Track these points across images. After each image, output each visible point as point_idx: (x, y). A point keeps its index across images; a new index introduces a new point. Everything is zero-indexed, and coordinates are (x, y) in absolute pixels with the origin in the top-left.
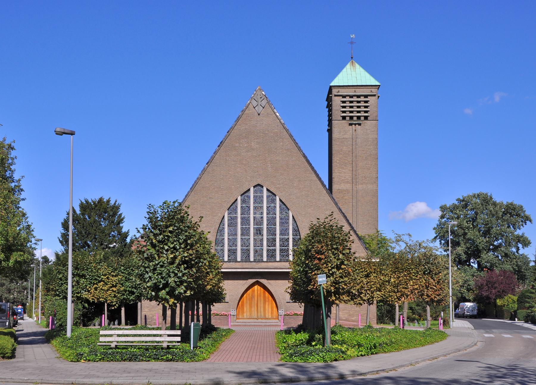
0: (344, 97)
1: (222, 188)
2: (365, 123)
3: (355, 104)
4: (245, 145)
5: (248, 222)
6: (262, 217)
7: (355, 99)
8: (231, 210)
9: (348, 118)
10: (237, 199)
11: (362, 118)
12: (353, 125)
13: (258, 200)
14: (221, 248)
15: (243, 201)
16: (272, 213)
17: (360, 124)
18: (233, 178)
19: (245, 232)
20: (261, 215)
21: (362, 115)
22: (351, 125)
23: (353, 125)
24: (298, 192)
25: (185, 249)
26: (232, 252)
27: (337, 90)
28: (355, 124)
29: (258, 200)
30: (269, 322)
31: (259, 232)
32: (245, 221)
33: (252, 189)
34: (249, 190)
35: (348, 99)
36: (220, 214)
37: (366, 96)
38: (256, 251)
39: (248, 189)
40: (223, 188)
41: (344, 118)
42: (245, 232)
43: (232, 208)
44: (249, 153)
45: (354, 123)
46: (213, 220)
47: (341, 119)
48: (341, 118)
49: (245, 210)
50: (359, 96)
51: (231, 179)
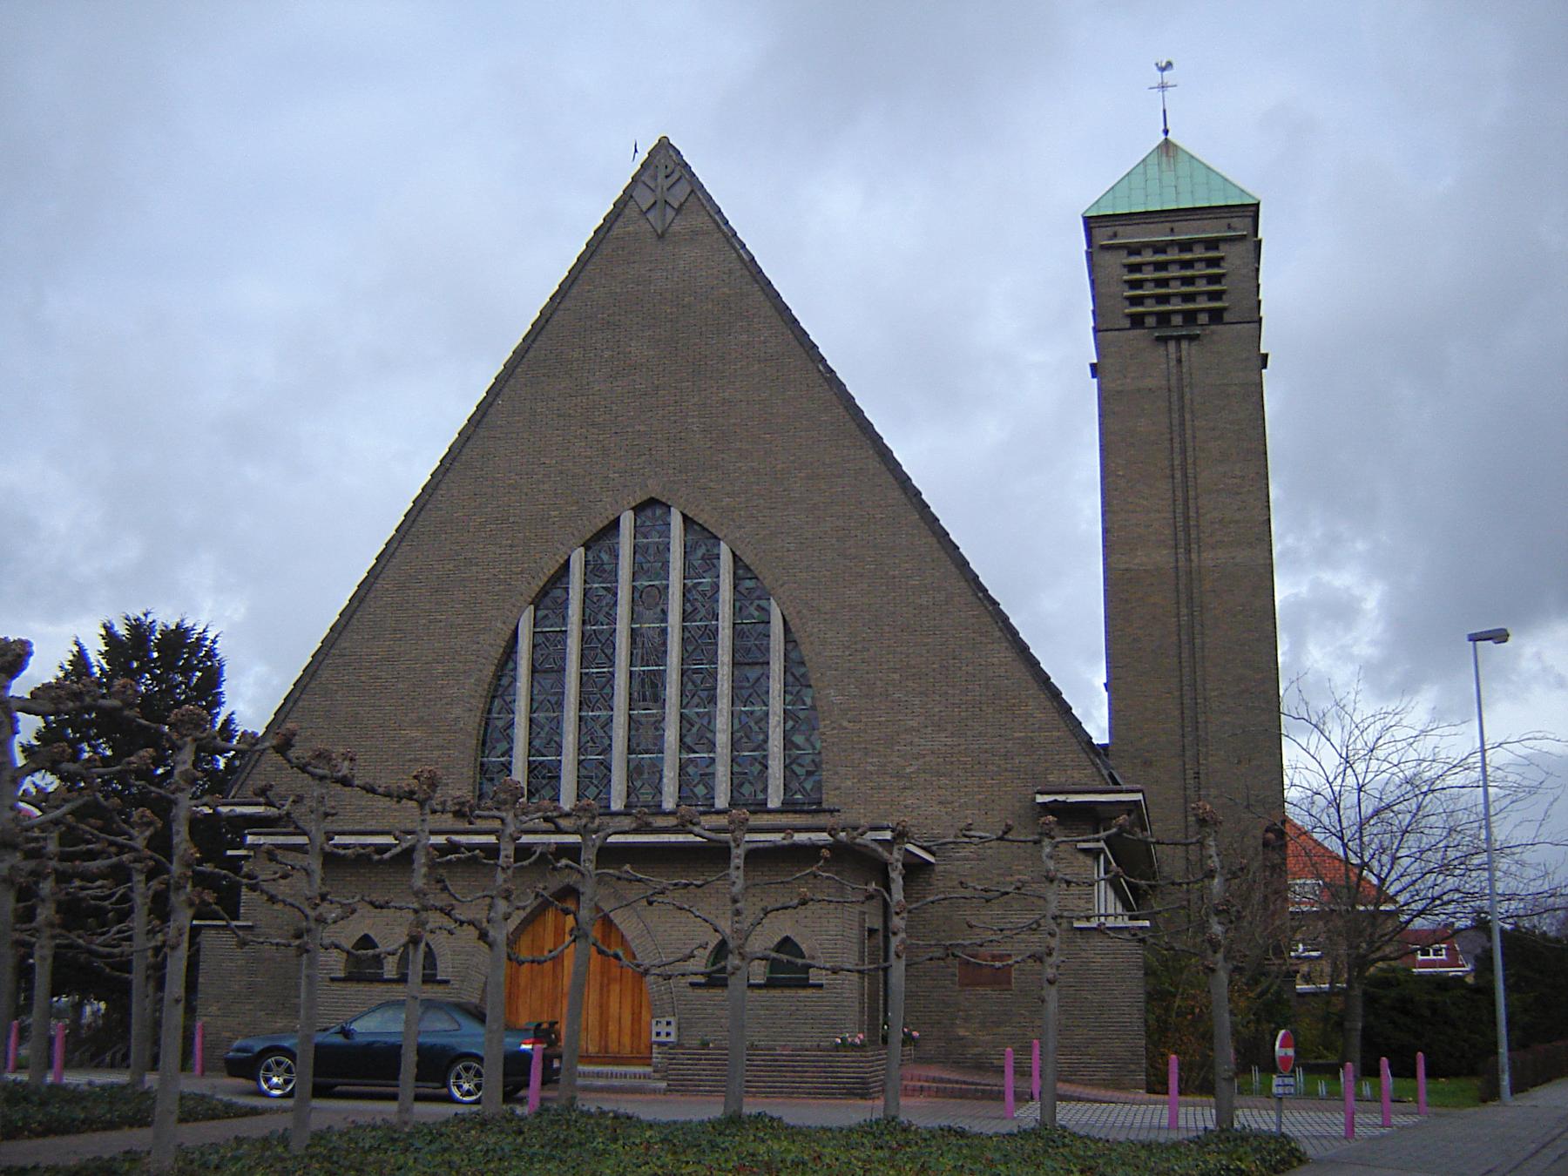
0: (1134, 250)
1: (511, 520)
2: (1213, 332)
3: (1174, 272)
4: (607, 354)
5: (609, 652)
6: (664, 631)
7: (1173, 255)
8: (547, 608)
9: (1151, 321)
10: (568, 561)
11: (1203, 318)
12: (1172, 345)
13: (650, 561)
14: (502, 759)
15: (594, 570)
16: (703, 612)
17: (1192, 338)
18: (555, 482)
19: (595, 693)
20: (662, 621)
21: (1149, 276)
22: (1163, 340)
23: (1172, 345)
24: (807, 523)
25: (1434, 955)
26: (543, 778)
27: (1110, 231)
28: (1178, 339)
29: (650, 561)
30: (613, 1075)
31: (648, 689)
32: (597, 647)
33: (627, 521)
34: (615, 524)
35: (1148, 256)
36: (499, 625)
37: (1212, 244)
38: (633, 772)
39: (612, 518)
40: (517, 519)
41: (1137, 321)
42: (595, 693)
43: (550, 595)
44: (619, 383)
45: (1175, 334)
46: (475, 647)
47: (1128, 326)
48: (1127, 323)
49: (598, 608)
50: (1186, 246)
51: (546, 487)
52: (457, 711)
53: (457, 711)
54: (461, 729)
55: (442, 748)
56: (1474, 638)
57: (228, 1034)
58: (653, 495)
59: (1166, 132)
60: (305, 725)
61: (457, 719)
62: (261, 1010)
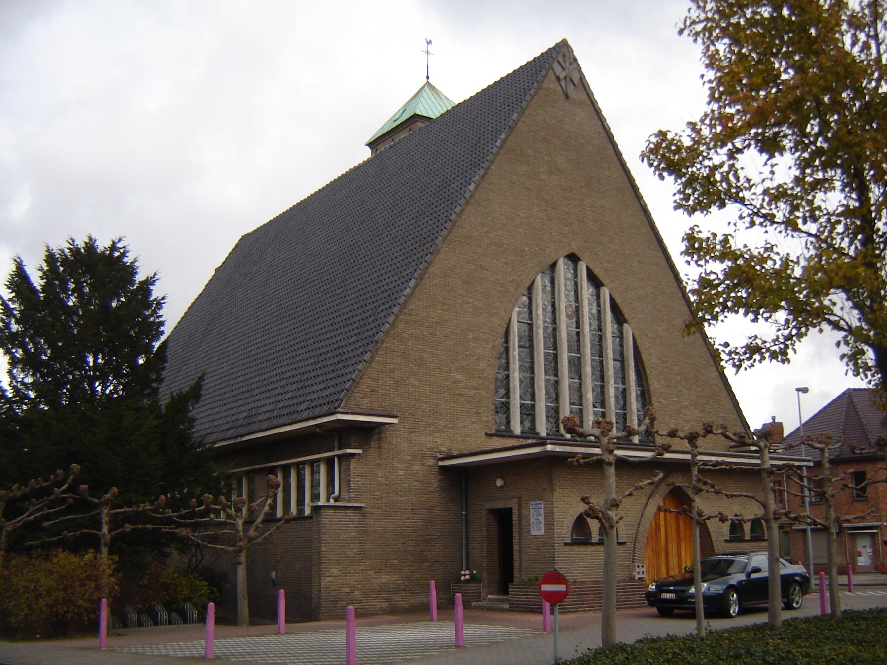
10: (533, 282)
52: (483, 365)
53: (483, 365)
54: (486, 377)
55: (475, 388)
56: (798, 390)
57: (348, 590)
58: (574, 251)
59: (428, 78)
60: (388, 360)
61: (483, 371)
62: (370, 570)
